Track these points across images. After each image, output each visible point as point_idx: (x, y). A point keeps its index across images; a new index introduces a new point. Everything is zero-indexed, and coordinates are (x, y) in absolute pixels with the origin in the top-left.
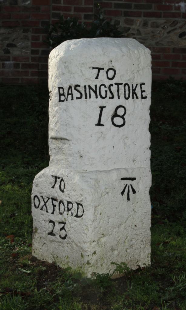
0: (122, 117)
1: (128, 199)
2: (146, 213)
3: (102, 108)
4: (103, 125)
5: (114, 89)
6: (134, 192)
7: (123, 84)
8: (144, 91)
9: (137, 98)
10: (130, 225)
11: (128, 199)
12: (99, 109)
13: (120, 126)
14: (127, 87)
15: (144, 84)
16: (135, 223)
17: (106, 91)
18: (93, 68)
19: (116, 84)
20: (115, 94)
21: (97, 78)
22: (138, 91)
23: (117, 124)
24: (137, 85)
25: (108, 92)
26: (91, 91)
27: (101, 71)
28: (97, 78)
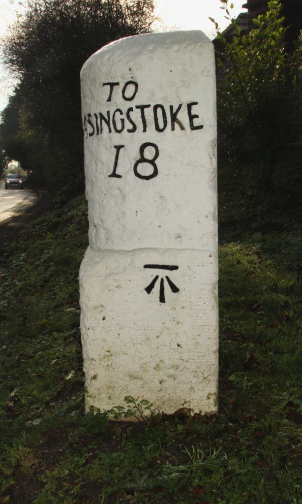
0: (152, 162)
1: (162, 299)
2: (202, 327)
3: (118, 148)
4: (119, 177)
5: (136, 115)
6: (175, 289)
7: (152, 106)
8: (197, 116)
9: (182, 128)
10: (168, 344)
11: (162, 299)
12: (115, 150)
13: (147, 178)
14: (159, 110)
15: (196, 103)
16: (179, 341)
17: (123, 121)
18: (104, 84)
19: (137, 107)
20: (140, 126)
21: (109, 100)
22: (183, 116)
23: (143, 174)
24: (180, 106)
25: (127, 122)
26: (103, 121)
27: (115, 87)
28: (109, 100)
